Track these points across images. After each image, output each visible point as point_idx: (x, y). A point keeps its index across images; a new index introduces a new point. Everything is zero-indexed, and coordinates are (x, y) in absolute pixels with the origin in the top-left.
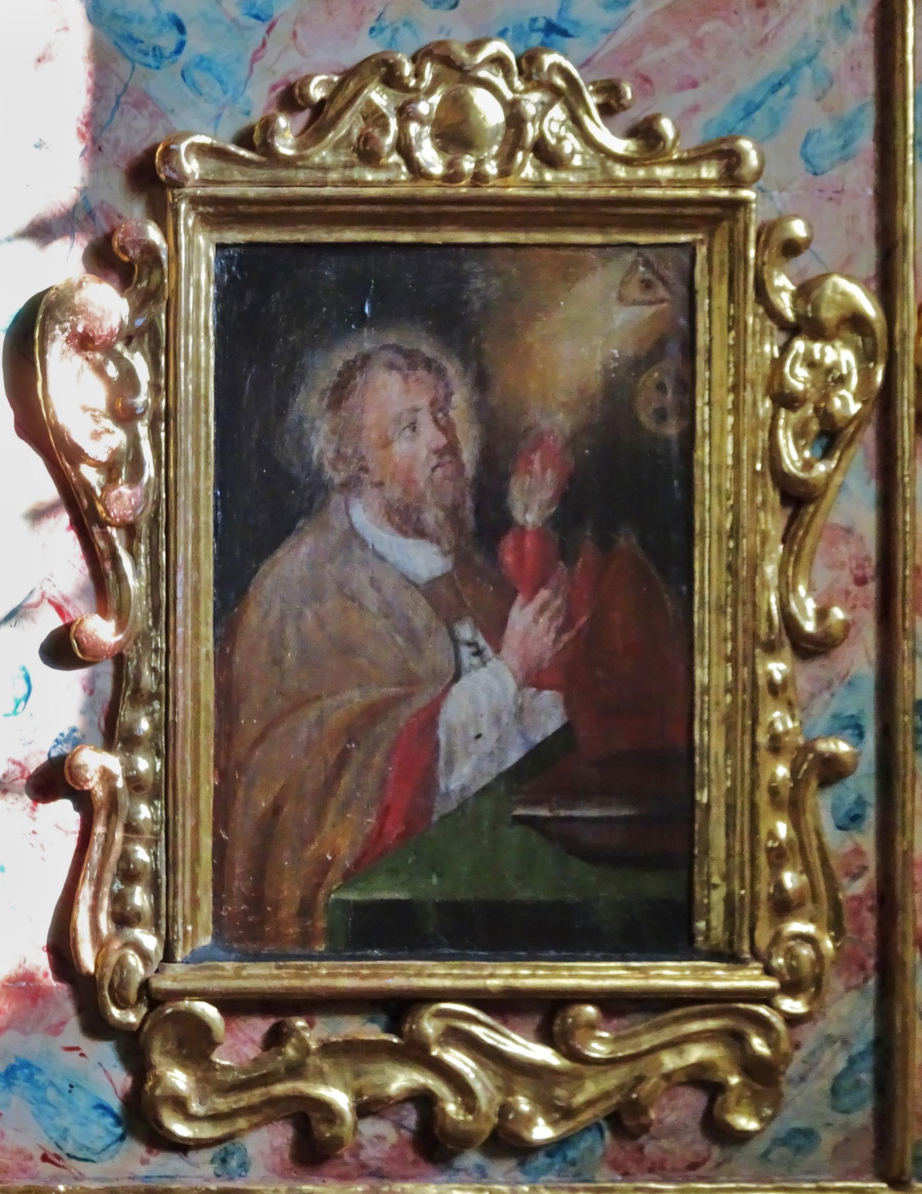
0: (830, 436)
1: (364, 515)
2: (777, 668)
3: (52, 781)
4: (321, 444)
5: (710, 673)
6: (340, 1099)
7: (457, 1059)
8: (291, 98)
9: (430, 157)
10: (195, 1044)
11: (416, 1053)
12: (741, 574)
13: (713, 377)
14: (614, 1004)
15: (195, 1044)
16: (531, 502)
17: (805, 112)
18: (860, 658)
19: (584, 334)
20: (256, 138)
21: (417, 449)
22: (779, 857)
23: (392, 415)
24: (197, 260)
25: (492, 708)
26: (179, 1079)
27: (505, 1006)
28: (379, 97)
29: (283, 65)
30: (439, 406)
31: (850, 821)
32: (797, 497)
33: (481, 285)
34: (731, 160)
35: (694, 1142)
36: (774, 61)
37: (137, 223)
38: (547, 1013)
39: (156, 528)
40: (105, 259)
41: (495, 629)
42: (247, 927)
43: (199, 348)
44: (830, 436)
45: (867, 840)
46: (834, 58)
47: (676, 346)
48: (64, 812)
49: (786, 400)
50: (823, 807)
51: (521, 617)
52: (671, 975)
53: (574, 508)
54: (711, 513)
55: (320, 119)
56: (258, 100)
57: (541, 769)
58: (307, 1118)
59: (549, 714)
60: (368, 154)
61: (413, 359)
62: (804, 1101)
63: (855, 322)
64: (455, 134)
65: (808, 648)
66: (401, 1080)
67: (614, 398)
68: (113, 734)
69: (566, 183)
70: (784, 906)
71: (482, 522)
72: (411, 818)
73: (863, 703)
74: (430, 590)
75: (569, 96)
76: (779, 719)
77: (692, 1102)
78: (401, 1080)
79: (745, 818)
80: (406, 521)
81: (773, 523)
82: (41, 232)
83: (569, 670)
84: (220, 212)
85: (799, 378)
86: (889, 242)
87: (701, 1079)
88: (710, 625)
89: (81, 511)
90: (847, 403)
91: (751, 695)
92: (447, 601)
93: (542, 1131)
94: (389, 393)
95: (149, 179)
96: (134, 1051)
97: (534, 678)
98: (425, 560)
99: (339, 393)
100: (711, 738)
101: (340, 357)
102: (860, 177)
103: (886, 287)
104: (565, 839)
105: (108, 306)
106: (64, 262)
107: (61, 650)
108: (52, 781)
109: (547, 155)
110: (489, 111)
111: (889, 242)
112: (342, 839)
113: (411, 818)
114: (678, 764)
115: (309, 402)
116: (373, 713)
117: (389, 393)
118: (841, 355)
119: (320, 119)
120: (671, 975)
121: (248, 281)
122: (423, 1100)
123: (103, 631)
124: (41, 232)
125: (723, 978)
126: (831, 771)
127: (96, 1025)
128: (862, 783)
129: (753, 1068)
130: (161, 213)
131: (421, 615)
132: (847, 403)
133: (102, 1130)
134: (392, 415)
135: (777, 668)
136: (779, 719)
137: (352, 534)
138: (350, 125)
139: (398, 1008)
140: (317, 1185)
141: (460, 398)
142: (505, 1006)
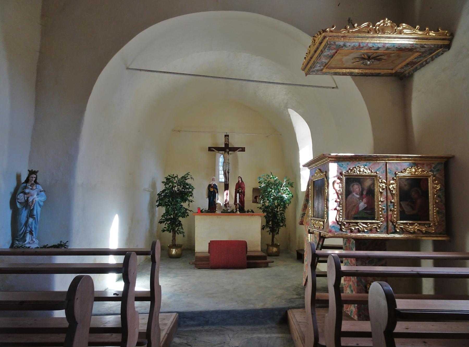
0: (383, 189)
1: (354, 194)
2: (380, 203)
3: (335, 209)
4: (352, 189)
5: (376, 203)
6: (353, 229)
7: (361, 226)
8: (350, 169)
9: (358, 173)
10: (344, 225)
11: (358, 226)
12: (378, 198)
13: (376, 186)
14: (370, 223)
15: (344, 225)
16: (365, 193)
17: (381, 170)
18: (385, 202)
19: (368, 183)
20: (348, 171)
21: (357, 190)
22: (380, 214)
23: (356, 188)
24: (344, 178)
25: (362, 205)
26: (343, 227)
27: (363, 223)
28: (355, 169)
29: (349, 167)
30: (359, 187)
31: (385, 212)
32: (381, 193)
33: (361, 180)
34: (377, 173)
35: (375, 232)
36: (379, 167)
37: (395, 214)
38: (366, 223)
39: (341, 194)
40: (339, 178)
41: (362, 200)
42: (347, 218)
43: (344, 184)
44: (383, 189)
45: (386, 213)
46: (383, 167)
47: (373, 184)
48: (336, 211)
49: (380, 187)
50: (383, 211)
51: (364, 200)
52: (374, 221)
53: (367, 194)
54: (376, 194)
55: (351, 170)
56: (348, 169)
57: (365, 209)
58: (351, 230)
59: (366, 206)
60: (354, 172)
61: (357, 184)
62: (382, 229)
63: (384, 183)
64: (360, 171)
65: (382, 202)
66: (357, 227)
67: (370, 187)
68: (339, 206)
69: (367, 174)
70: (381, 217)
71: (361, 194)
72: (358, 212)
73: (385, 205)
74: (358, 198)
75: (367, 169)
76: (380, 206)
77: (375, 229)
78: (357, 227)
79: (378, 212)
80: (357, 194)
81: (380, 194)
82: (334, 177)
83: (367, 203)
84: (345, 176)
85: (381, 186)
86: (387, 178)
87: (376, 228)
88: (376, 200)
89: (337, 193)
90: (384, 187)
91: (379, 205)
92: (359, 199)
93: (366, 231)
94: (356, 186)
95: (341, 174)
96: (340, 225)
97: (365, 203)
98: (358, 196)
99: (353, 186)
100: (376, 207)
101: (353, 184)
102: (385, 174)
103: (386, 180)
104: (367, 213)
105: (339, 181)
106: (336, 179)
107: (336, 201)
108: (335, 209)
109: (365, 173)
110: (362, 170)
111: (387, 178)
112: (353, 213)
113: (358, 212)
114: (374, 209)
115: (351, 187)
116: (355, 206)
117: (356, 186)
118: (384, 184)
119: (351, 170)
120: (374, 221)
121: (347, 180)
122: (358, 229)
123: (338, 200)
124: (334, 177)
125: (377, 222)
126: (383, 209)
127: (338, 224)
128: (385, 210)
129: (379, 227)
130: (342, 176)
131: (358, 199)
132: (384, 187)
133: (338, 230)
134: (356, 188)
135: (380, 203)
136: (380, 206)
137: (353, 195)
138: (353, 171)
139: (357, 223)
140: (261, 333)
141: (360, 187)
142: (363, 223)
